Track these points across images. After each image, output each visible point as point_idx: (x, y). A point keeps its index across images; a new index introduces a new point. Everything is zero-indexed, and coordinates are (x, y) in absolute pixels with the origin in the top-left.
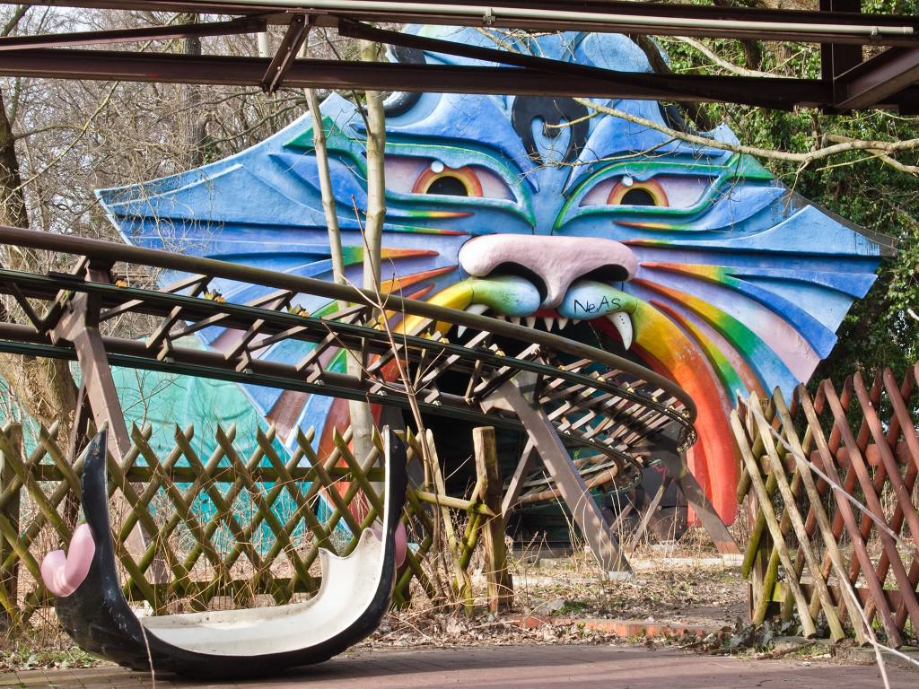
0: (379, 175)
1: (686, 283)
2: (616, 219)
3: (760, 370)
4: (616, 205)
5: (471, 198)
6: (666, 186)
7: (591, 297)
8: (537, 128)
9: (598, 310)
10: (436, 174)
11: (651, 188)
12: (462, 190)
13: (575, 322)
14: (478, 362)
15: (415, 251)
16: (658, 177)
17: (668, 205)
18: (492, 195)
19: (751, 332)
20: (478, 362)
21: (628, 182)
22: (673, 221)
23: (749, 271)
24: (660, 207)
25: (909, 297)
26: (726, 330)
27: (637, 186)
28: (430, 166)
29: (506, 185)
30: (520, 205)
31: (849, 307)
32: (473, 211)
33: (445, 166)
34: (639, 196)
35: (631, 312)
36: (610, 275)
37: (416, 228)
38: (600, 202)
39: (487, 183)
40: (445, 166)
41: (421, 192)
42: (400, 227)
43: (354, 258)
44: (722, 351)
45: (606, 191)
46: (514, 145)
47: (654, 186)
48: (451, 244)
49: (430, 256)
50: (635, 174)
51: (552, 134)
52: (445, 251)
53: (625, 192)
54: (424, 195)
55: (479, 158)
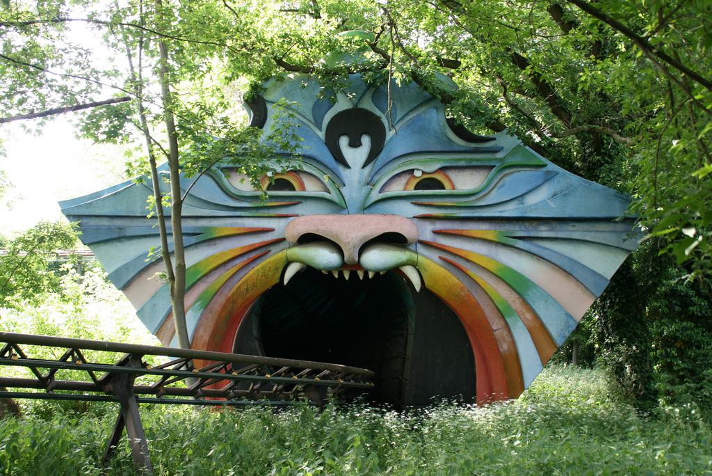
1: (473, 243)
2: (413, 201)
3: (534, 307)
4: (411, 191)
5: (298, 193)
6: (453, 175)
7: (377, 259)
8: (344, 141)
10: (418, 177)
12: (291, 187)
13: (371, 275)
14: (662, 209)
15: (254, 228)
16: (442, 169)
17: (454, 188)
18: (311, 188)
20: (662, 209)
25: (626, 330)
26: (447, 299)
28: (413, 173)
30: (333, 196)
32: (301, 200)
35: (414, 265)
36: (393, 240)
37: (243, 214)
38: (397, 188)
42: (243, 214)
44: (502, 293)
45: (404, 180)
46: (327, 157)
47: (441, 175)
49: (271, 230)
51: (355, 144)
52: (279, 227)
53: (417, 181)
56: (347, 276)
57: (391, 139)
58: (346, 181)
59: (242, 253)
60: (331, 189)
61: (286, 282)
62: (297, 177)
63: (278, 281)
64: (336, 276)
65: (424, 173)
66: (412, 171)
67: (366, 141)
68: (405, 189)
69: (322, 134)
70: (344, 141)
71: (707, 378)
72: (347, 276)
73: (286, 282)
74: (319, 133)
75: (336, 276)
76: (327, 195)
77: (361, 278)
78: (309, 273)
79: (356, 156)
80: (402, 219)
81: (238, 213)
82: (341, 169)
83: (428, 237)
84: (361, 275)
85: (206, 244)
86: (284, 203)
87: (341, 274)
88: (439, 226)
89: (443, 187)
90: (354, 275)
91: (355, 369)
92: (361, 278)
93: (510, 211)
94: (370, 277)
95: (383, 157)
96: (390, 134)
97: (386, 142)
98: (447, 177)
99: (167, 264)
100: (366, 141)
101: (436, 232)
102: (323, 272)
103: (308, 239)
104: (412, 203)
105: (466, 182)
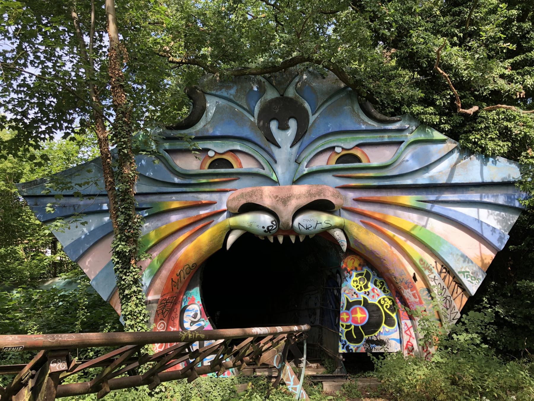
0: (247, 156)
4: (333, 165)
6: (367, 150)
8: (274, 125)
9: (315, 228)
11: (357, 152)
16: (359, 146)
18: (247, 165)
19: (438, 236)
21: (338, 150)
22: (207, 177)
23: (432, 197)
24: (364, 164)
27: (217, 157)
29: (257, 160)
30: (266, 171)
31: (516, 219)
32: (240, 177)
33: (215, 152)
34: (349, 158)
37: (184, 189)
38: (321, 163)
39: (242, 159)
40: (215, 152)
41: (204, 169)
43: (160, 208)
45: (325, 157)
46: (260, 139)
48: (476, 193)
49: (357, 200)
50: (342, 145)
51: (283, 127)
53: (210, 161)
54: (206, 170)
55: (238, 146)
56: (281, 239)
57: (315, 121)
58: (277, 158)
59: (188, 223)
60: (265, 166)
61: (228, 247)
62: (234, 157)
63: (221, 247)
64: (272, 241)
65: (343, 149)
66: (333, 148)
67: (293, 124)
68: (201, 168)
69: (254, 120)
70: (274, 125)
71: (442, 371)
72: (281, 239)
73: (228, 247)
74: (252, 119)
75: (272, 241)
76: (261, 171)
77: (293, 242)
78: (248, 237)
79: (285, 137)
80: (329, 188)
81: (184, 189)
82: (274, 148)
83: (350, 204)
84: (293, 239)
85: (482, 188)
86: (224, 179)
87: (276, 239)
88: (365, 195)
89: (360, 161)
90: (287, 239)
91: (279, 329)
92: (293, 242)
93: (422, 179)
94: (301, 240)
95: (307, 139)
96: (312, 119)
97: (310, 125)
98: (237, 159)
99: (401, 210)
100: (293, 124)
101: (357, 200)
102: (261, 238)
103: (250, 208)
104: (333, 176)
105: (376, 157)
